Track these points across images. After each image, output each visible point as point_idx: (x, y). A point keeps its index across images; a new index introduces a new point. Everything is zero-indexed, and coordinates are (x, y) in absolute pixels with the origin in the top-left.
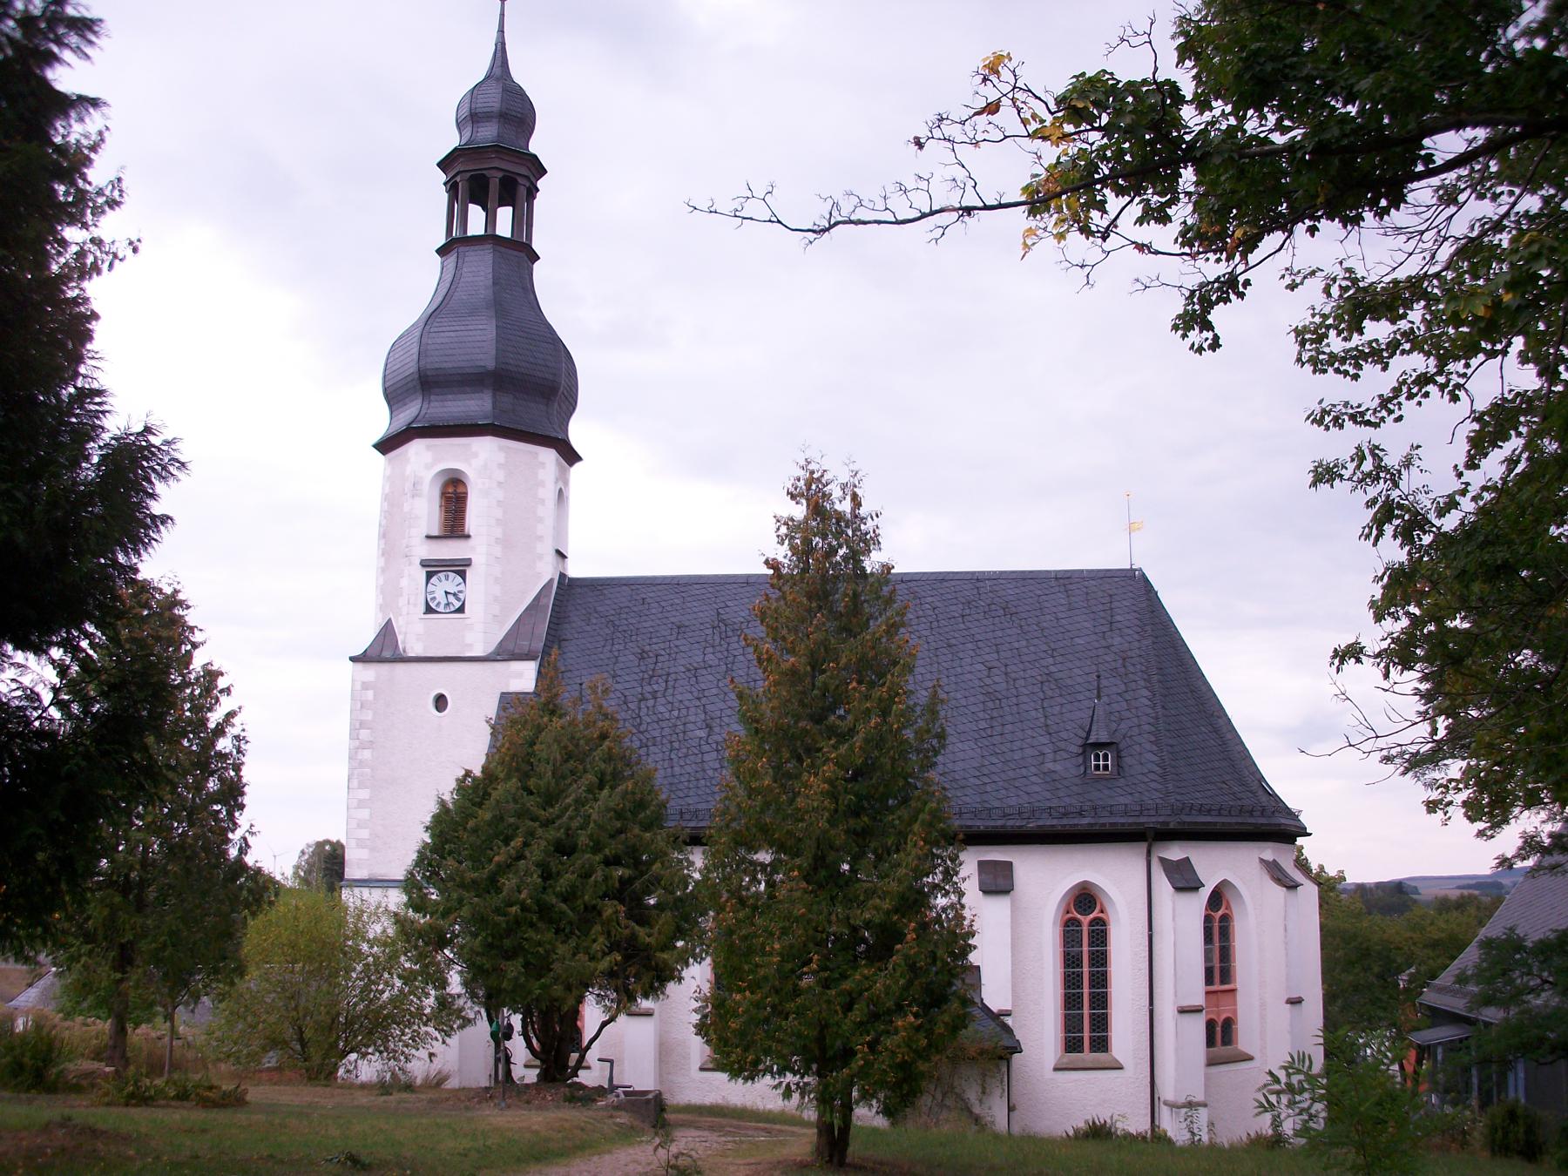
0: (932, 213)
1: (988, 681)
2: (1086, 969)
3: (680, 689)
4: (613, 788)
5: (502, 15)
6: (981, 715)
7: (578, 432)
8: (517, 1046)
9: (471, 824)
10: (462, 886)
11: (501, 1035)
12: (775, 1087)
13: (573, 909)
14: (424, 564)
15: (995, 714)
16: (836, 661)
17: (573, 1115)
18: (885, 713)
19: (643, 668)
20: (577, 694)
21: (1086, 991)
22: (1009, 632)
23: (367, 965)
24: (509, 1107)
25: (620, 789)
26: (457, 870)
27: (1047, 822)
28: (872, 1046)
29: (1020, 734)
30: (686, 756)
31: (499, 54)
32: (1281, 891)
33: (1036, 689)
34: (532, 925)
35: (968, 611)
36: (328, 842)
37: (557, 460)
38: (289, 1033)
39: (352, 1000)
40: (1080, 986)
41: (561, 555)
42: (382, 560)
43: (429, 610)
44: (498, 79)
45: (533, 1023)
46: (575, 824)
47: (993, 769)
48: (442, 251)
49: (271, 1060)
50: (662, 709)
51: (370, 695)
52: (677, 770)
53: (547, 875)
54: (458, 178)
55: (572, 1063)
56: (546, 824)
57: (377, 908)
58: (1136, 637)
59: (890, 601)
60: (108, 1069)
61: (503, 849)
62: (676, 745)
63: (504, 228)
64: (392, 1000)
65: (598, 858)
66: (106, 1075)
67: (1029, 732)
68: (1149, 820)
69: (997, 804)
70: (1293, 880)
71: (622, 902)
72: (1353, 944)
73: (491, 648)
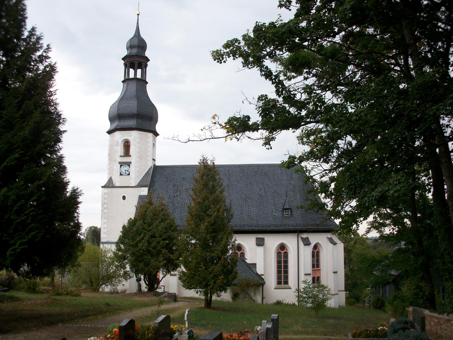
0: (206, 139)
1: (260, 192)
2: (282, 264)
3: (184, 195)
4: (164, 222)
5: (138, 19)
6: (258, 201)
7: (158, 128)
8: (142, 283)
9: (131, 231)
10: (129, 245)
11: (139, 280)
12: (195, 291)
13: (155, 251)
14: (120, 163)
15: (261, 201)
16: (208, 200)
17: (155, 298)
18: (219, 211)
19: (174, 189)
20: (158, 196)
21: (283, 269)
22: (266, 180)
23: (107, 264)
24: (140, 297)
25: (166, 222)
26: (128, 242)
27: (273, 228)
28: (215, 282)
29: (267, 206)
30: (185, 211)
31: (137, 30)
32: (332, 245)
33: (272, 194)
34: (146, 255)
35: (256, 174)
36: (94, 227)
37: (153, 136)
38: (88, 280)
39: (104, 273)
40: (281, 268)
41: (154, 160)
42: (109, 161)
43: (121, 175)
44: (137, 37)
45: (146, 277)
46: (156, 231)
47: (260, 214)
48: (123, 82)
49: (84, 286)
50: (179, 199)
51: (106, 196)
52: (182, 215)
53: (149, 243)
54: (127, 63)
55: (155, 287)
56: (149, 231)
57: (110, 249)
58: (298, 181)
59: (221, 186)
60: (50, 288)
61: (139, 237)
62: (182, 208)
63: (139, 76)
64: (113, 272)
65: (161, 239)
66: (51, 289)
67: (270, 205)
68: (298, 228)
69: (261, 224)
70: (335, 242)
71: (167, 249)
72: (363, 257)
73: (137, 184)
